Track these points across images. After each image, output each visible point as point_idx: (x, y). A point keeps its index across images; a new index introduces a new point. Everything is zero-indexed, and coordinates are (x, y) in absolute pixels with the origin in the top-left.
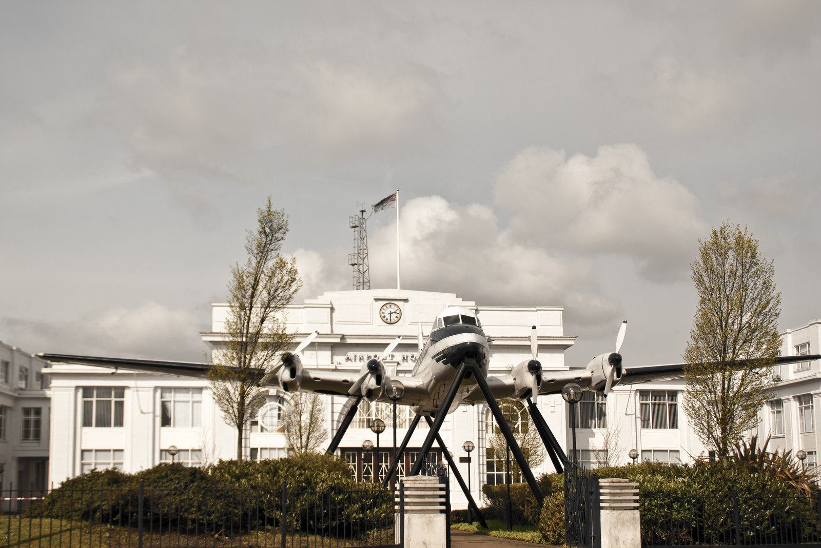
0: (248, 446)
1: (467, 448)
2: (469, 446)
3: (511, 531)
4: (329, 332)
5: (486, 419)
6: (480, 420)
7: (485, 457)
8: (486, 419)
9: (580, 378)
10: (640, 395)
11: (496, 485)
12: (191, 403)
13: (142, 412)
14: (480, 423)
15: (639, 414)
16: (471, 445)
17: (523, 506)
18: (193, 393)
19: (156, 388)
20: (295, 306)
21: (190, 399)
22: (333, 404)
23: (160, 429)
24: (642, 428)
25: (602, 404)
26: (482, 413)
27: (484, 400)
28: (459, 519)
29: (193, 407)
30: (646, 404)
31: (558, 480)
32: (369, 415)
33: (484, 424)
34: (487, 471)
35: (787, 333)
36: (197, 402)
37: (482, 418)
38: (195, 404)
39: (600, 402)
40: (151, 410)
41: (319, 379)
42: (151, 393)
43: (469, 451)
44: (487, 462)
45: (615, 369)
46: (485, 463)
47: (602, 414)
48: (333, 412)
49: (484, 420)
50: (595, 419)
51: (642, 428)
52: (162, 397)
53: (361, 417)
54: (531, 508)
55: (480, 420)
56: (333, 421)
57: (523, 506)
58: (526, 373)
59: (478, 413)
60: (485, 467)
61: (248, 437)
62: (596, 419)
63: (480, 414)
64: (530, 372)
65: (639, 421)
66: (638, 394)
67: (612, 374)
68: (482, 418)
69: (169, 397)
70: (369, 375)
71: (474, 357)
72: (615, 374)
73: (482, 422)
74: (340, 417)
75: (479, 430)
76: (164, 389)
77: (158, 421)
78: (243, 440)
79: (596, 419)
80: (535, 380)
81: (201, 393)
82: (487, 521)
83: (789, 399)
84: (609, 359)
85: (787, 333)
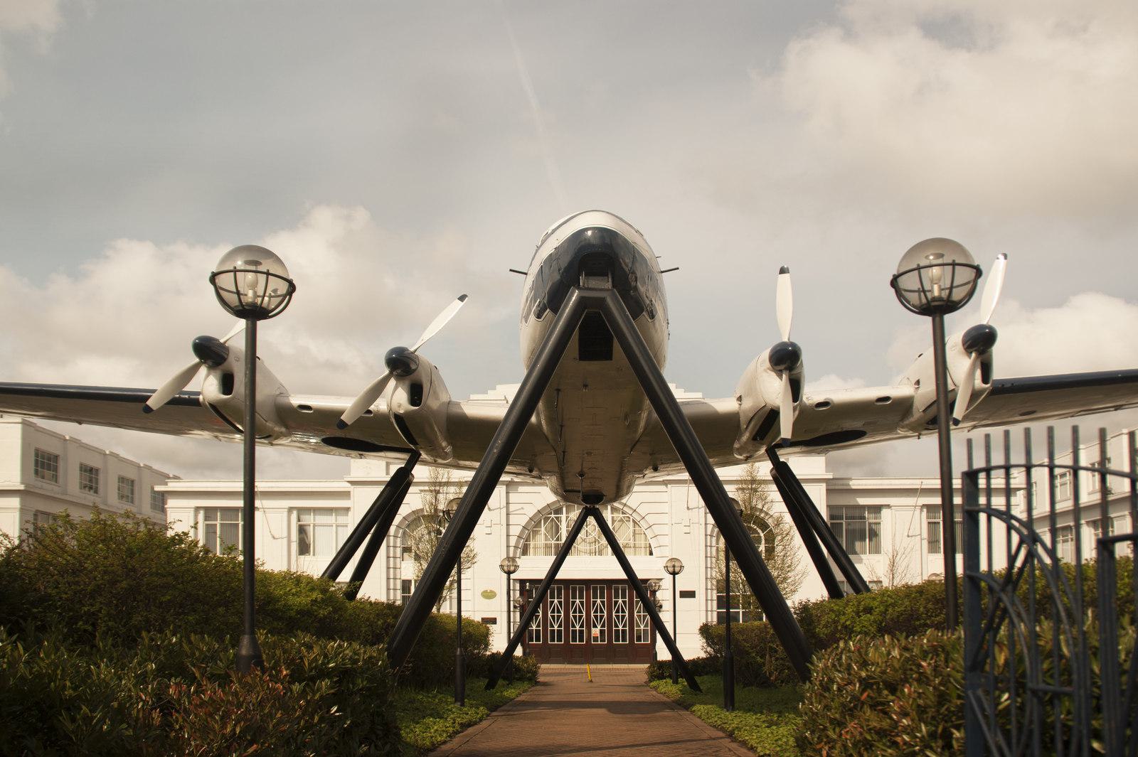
0: (399, 577)
1: (671, 569)
2: (674, 566)
3: (733, 710)
4: (270, 276)
5: (717, 543)
6: (709, 544)
7: (715, 592)
8: (717, 543)
9: (887, 399)
10: (928, 512)
11: (741, 622)
12: (334, 528)
13: (274, 538)
14: (709, 548)
15: (925, 534)
16: (677, 564)
17: (763, 656)
18: (336, 515)
19: (291, 509)
20: (492, 402)
21: (334, 521)
22: (508, 525)
23: (297, 557)
24: (929, 552)
25: (876, 523)
26: (711, 536)
27: (677, 461)
28: (663, 673)
29: (337, 533)
30: (935, 523)
31: (838, 611)
32: (557, 540)
33: (714, 549)
34: (718, 608)
35: (1122, 434)
36: (342, 526)
37: (711, 541)
38: (339, 528)
39: (871, 521)
40: (285, 534)
41: (308, 408)
42: (285, 514)
43: (253, 313)
44: (718, 596)
45: (978, 363)
46: (715, 598)
47: (874, 534)
48: (508, 536)
49: (714, 544)
50: (865, 540)
51: (929, 552)
52: (299, 520)
53: (548, 542)
54: (777, 659)
55: (709, 544)
56: (508, 546)
57: (763, 656)
58: (765, 374)
59: (706, 535)
60: (715, 603)
61: (398, 566)
62: (867, 540)
63: (709, 537)
64: (774, 370)
65: (925, 543)
66: (925, 510)
67: (971, 374)
68: (711, 541)
69: (308, 519)
70: (392, 383)
71: (607, 275)
72: (978, 373)
73: (711, 546)
74: (518, 542)
75: (706, 557)
76: (301, 511)
77: (295, 547)
78: (512, 592)
79: (867, 540)
80: (786, 385)
81: (348, 516)
82: (698, 679)
83: (1124, 516)
84: (964, 343)
85: (1122, 434)
